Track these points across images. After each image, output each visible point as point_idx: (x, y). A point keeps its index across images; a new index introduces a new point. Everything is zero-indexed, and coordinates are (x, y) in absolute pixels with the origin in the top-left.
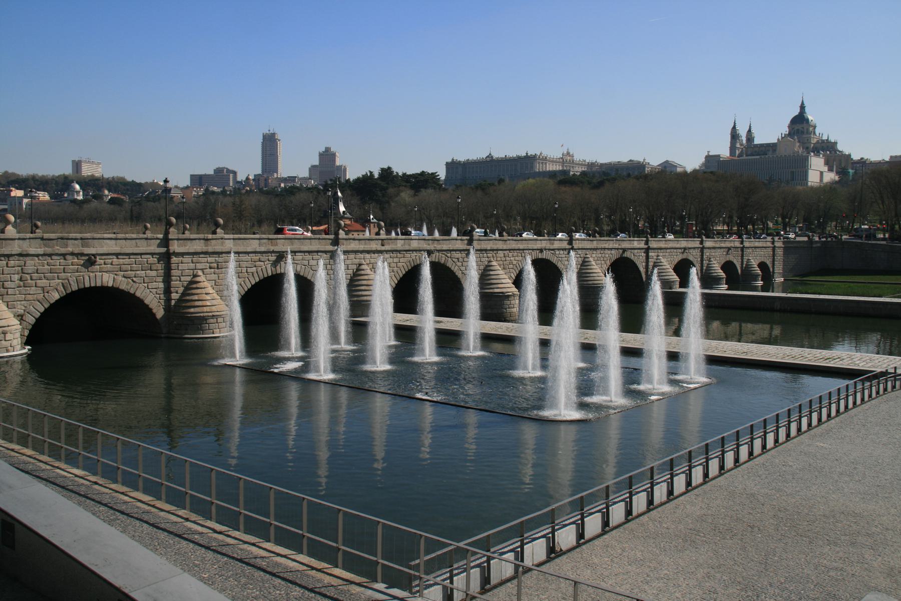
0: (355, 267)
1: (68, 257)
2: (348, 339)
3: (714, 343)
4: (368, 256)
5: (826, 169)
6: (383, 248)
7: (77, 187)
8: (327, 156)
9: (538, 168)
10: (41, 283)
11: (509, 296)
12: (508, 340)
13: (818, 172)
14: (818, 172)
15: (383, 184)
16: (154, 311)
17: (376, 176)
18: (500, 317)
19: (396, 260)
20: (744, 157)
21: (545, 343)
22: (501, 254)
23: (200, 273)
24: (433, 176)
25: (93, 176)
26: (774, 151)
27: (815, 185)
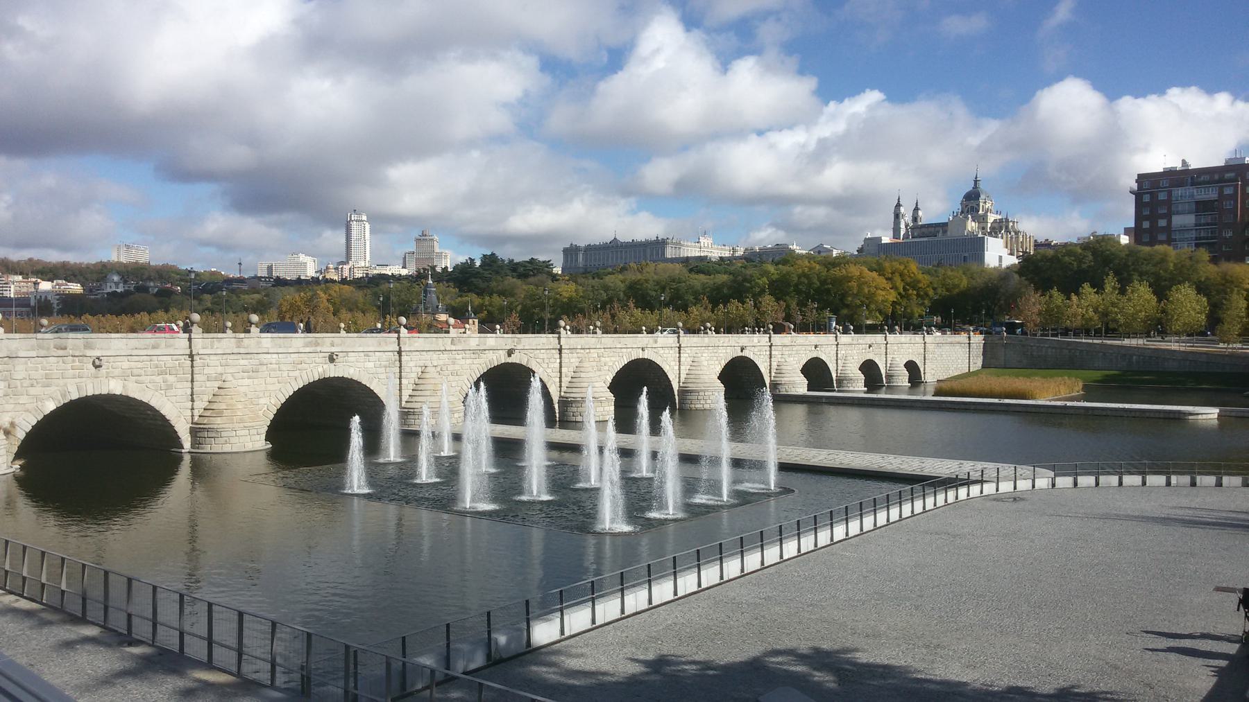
0: (420, 370)
2: (492, 460)
3: (789, 450)
4: (435, 356)
5: (1006, 251)
6: (453, 348)
7: (116, 278)
8: (1233, 103)
9: (670, 253)
10: (32, 391)
11: (571, 402)
12: (575, 448)
13: (998, 255)
14: (998, 255)
15: (486, 274)
16: (173, 423)
17: (478, 263)
18: (566, 423)
19: (468, 361)
20: (910, 239)
21: (654, 455)
22: (594, 353)
23: (229, 378)
24: (547, 265)
25: (136, 263)
26: (945, 232)
27: (992, 266)
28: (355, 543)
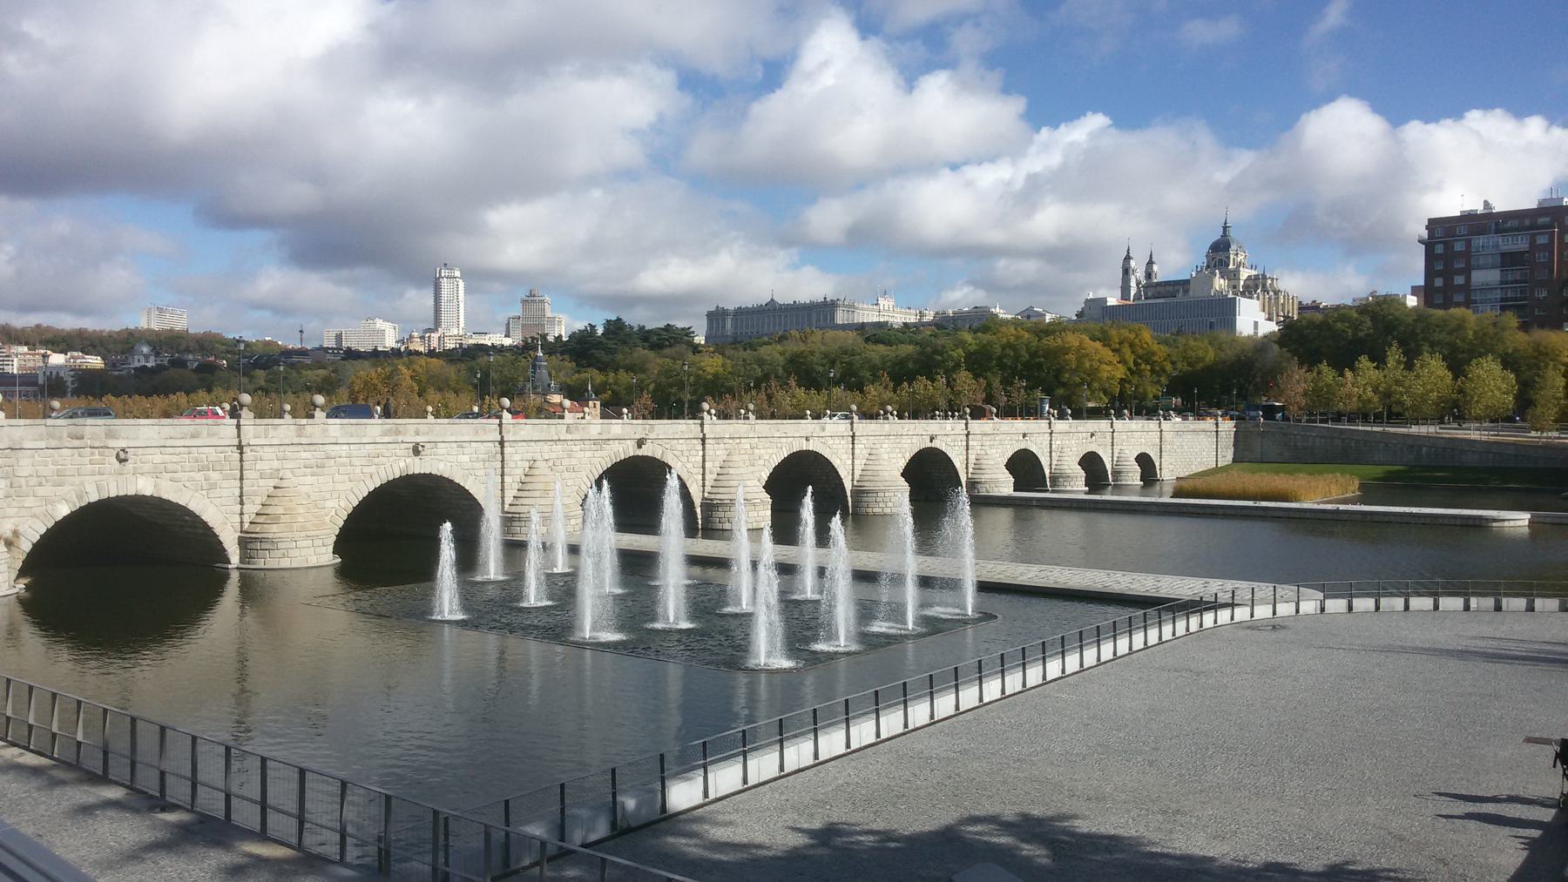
0: (527, 465)
1: (1376, 403)
3: (990, 565)
4: (546, 447)
5: (1264, 315)
6: (569, 437)
7: (145, 349)
9: (841, 317)
10: (41, 491)
11: (717, 505)
12: (722, 563)
13: (1252, 320)
14: (1252, 320)
15: (611, 344)
16: (217, 531)
17: (600, 331)
18: (710, 531)
19: (588, 454)
20: (1143, 300)
21: (821, 572)
22: (746, 444)
23: (288, 474)
24: (687, 333)
25: (171, 330)
26: (1186, 291)
28: (446, 682)
